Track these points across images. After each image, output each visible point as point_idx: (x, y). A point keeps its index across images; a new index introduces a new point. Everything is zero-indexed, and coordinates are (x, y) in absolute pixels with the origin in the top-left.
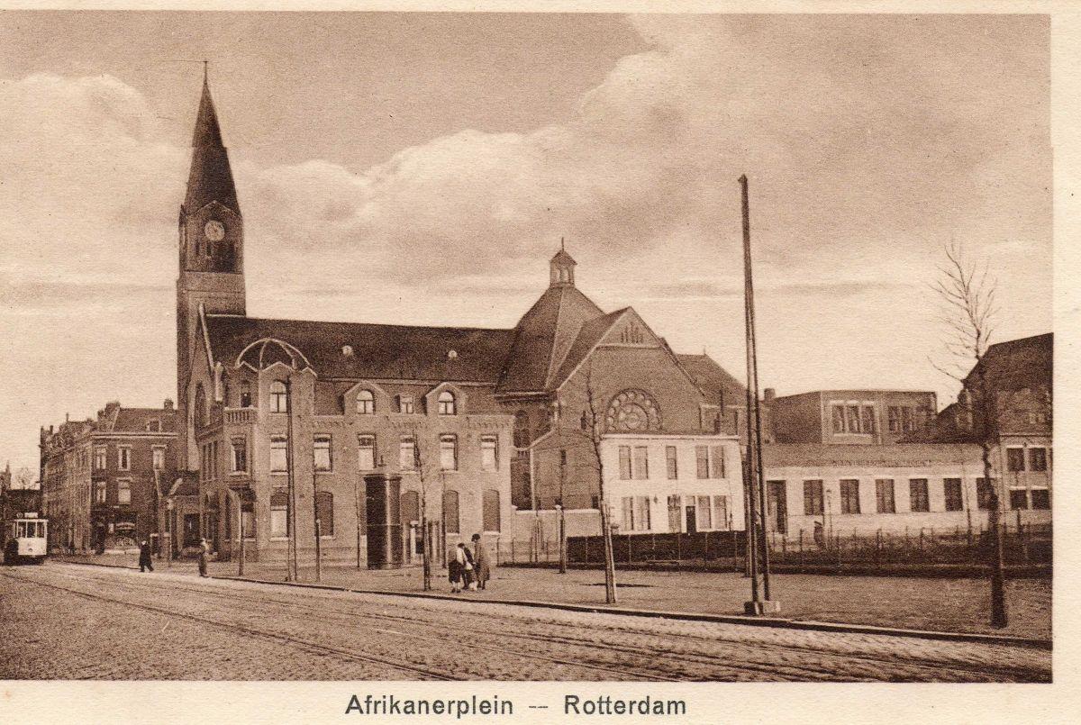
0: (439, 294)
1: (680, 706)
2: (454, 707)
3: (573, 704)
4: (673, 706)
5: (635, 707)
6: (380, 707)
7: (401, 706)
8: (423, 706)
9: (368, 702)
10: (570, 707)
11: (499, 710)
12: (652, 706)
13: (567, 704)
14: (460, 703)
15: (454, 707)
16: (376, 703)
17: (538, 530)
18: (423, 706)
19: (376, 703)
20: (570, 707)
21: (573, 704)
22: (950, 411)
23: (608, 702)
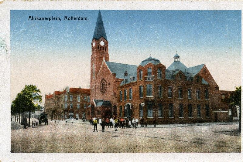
0: (139, 126)
1: (86, 19)
2: (49, 19)
3: (66, 18)
4: (85, 19)
5: (78, 19)
6: (35, 19)
7: (39, 19)
8: (43, 19)
9: (32, 18)
10: (66, 19)
11: (57, 19)
12: (81, 18)
13: (65, 18)
14: (50, 18)
15: (49, 19)
16: (34, 18)
17: (39, 97)
18: (43, 19)
19: (34, 18)
20: (66, 19)
21: (66, 18)
22: (195, 116)
23: (73, 18)
